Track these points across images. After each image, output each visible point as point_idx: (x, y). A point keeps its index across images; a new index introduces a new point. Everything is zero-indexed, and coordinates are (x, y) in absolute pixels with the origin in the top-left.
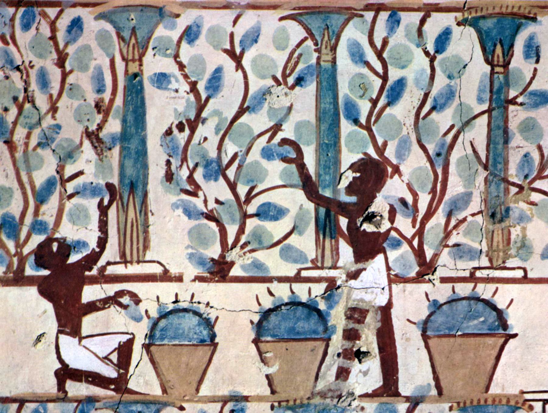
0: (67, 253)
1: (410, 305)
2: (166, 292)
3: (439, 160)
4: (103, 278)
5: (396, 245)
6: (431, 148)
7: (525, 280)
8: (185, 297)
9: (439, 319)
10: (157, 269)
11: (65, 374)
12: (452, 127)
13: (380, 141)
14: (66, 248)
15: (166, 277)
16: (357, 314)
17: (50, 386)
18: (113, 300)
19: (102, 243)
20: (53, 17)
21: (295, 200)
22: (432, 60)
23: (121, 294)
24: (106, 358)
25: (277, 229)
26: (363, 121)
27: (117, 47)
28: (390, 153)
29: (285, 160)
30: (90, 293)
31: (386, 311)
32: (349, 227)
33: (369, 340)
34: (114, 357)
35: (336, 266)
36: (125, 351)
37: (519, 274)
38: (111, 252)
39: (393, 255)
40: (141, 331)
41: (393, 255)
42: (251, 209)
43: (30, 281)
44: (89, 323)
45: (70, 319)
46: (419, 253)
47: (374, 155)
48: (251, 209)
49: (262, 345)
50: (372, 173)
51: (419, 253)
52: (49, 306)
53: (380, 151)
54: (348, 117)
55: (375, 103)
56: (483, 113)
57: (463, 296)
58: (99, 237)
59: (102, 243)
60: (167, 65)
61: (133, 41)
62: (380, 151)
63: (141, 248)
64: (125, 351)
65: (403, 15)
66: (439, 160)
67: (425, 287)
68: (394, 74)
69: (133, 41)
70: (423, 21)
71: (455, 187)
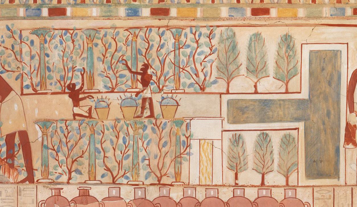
0: (333, 51)
1: (157, 98)
2: (99, 96)
4: (84, 93)
5: (152, 84)
7: (184, 93)
9: (164, 101)
10: (97, 91)
11: (75, 115)
12: (165, 54)
13: (148, 59)
14: (74, 85)
15: (99, 92)
16: (144, 100)
17: (72, 118)
19: (83, 84)
20: (72, 33)
22: (160, 38)
23: (89, 96)
24: (86, 111)
25: (124, 80)
26: (144, 54)
27: (86, 40)
28: (150, 62)
29: (123, 64)
30: (81, 96)
32: (141, 79)
34: (88, 111)
35: (113, 91)
36: (90, 110)
37: (183, 91)
38: (85, 88)
39: (152, 87)
41: (152, 87)
42: (117, 75)
44: (81, 103)
45: (76, 102)
46: (159, 87)
47: (146, 62)
49: (97, 109)
50: (146, 67)
51: (159, 87)
52: (71, 100)
53: (148, 61)
54: (139, 54)
55: (147, 50)
56: (173, 51)
59: (83, 84)
60: (99, 42)
61: (90, 38)
62: (148, 61)
63: (92, 85)
64: (90, 110)
65: (153, 29)
66: (163, 63)
67: (160, 94)
68: (151, 43)
69: (90, 38)
70: (159, 30)
71: (166, 69)
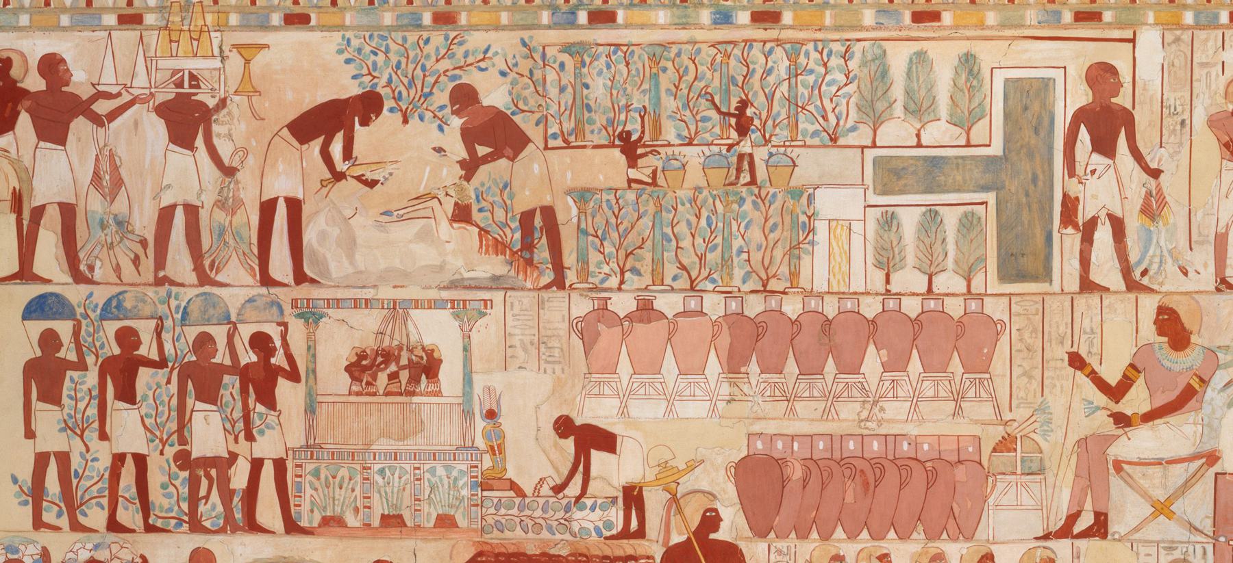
1: (760, 154)
2: (669, 150)
3: (770, 98)
4: (645, 146)
5: (753, 132)
6: (767, 91)
7: (805, 146)
8: (677, 152)
11: (630, 181)
14: (629, 134)
15: (669, 145)
16: (741, 157)
18: (651, 152)
19: (643, 132)
21: (713, 114)
25: (709, 125)
30: (640, 151)
31: (751, 155)
32: (737, 124)
33: (746, 166)
36: (654, 172)
39: (753, 136)
40: (660, 164)
41: (753, 136)
42: (698, 118)
43: (617, 146)
44: (640, 162)
46: (764, 136)
48: (698, 118)
50: (744, 104)
51: (764, 136)
52: (624, 157)
53: (746, 96)
57: (1157, 422)
58: (365, 122)
59: (643, 132)
60: (669, 65)
62: (746, 96)
64: (654, 172)
68: (751, 67)
